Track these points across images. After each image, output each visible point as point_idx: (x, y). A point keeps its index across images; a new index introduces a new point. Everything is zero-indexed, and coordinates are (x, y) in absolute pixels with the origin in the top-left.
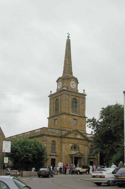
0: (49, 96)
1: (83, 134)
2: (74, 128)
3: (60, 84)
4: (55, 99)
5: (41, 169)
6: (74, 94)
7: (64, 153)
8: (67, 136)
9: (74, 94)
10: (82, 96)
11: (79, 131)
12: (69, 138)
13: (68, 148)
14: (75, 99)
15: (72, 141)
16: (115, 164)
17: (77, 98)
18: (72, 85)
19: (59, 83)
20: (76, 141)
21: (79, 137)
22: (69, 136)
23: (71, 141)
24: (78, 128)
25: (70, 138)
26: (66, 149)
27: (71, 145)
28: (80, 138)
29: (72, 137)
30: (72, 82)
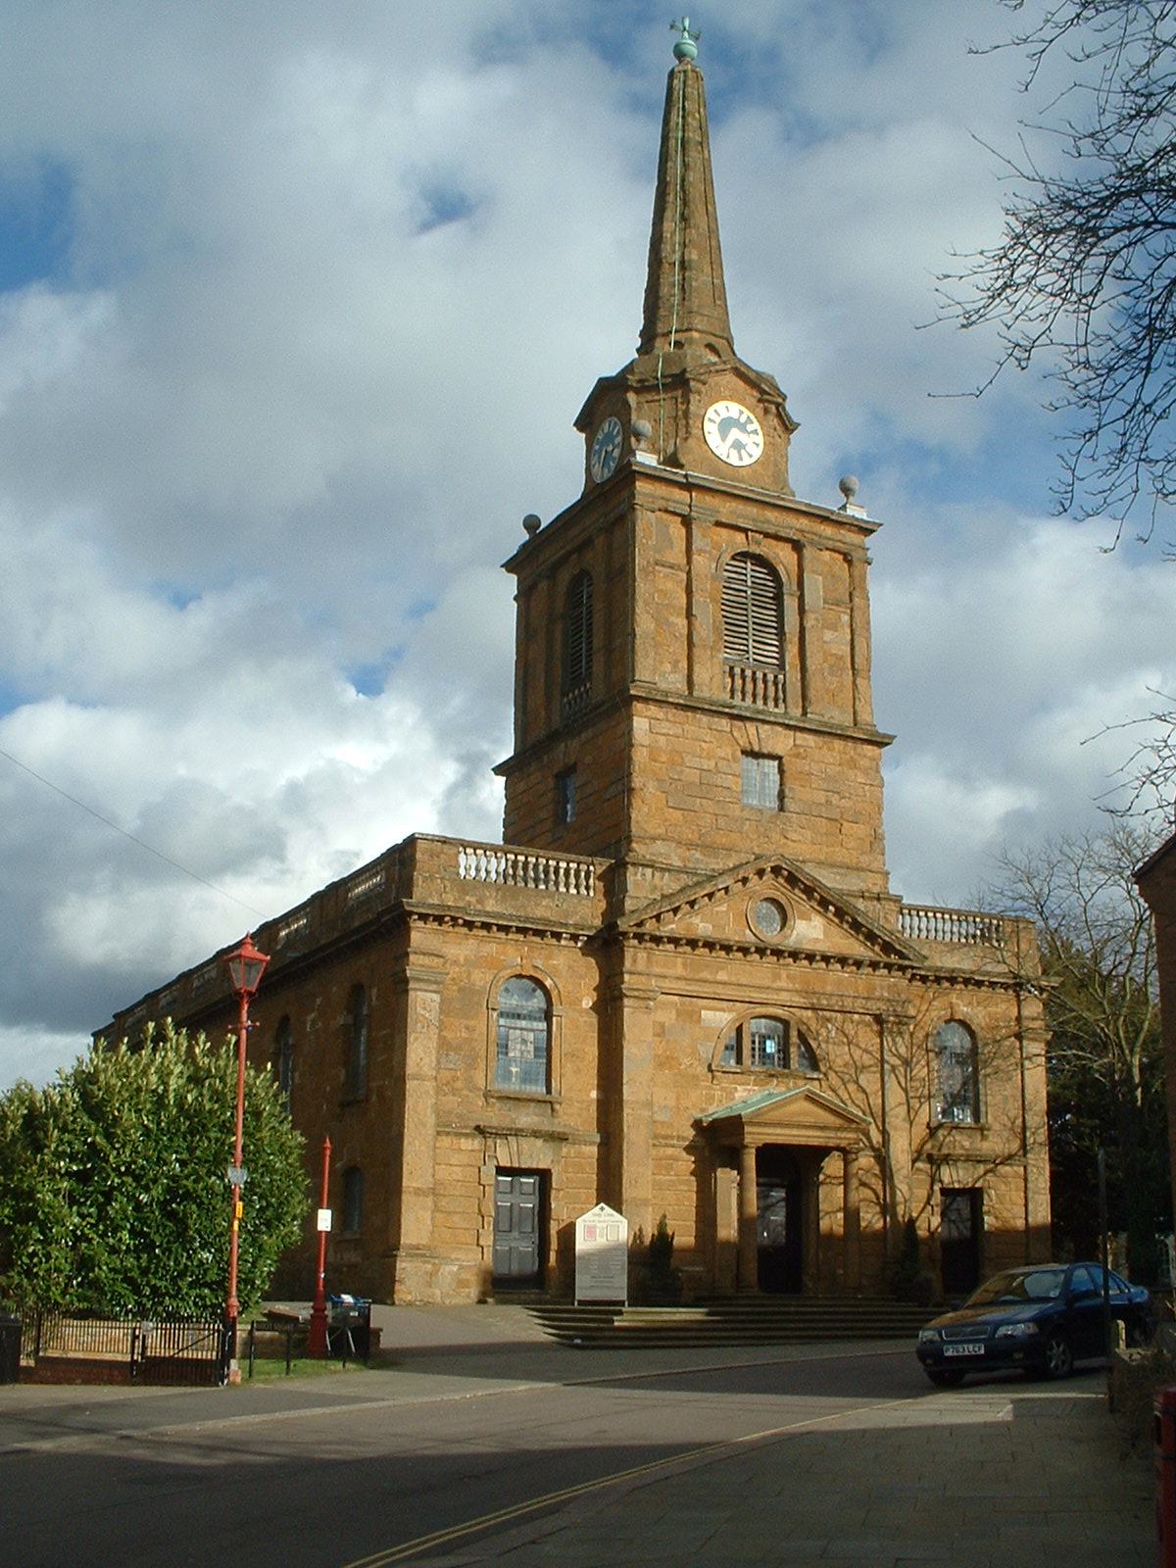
0: (511, 566)
1: (861, 904)
2: (749, 845)
3: (609, 438)
4: (565, 576)
5: (551, 962)
6: (745, 514)
7: (649, 1105)
8: (671, 927)
9: (745, 514)
10: (828, 530)
11: (808, 868)
12: (693, 943)
13: (694, 1052)
14: (760, 560)
15: (728, 971)
16: (327, 1301)
17: (783, 557)
18: (724, 435)
19: (600, 437)
20: (776, 977)
21: (811, 930)
22: (701, 926)
23: (722, 976)
24: (799, 845)
25: (710, 945)
26: (664, 1062)
27: (719, 1019)
28: (823, 947)
29: (734, 933)
30: (725, 409)
